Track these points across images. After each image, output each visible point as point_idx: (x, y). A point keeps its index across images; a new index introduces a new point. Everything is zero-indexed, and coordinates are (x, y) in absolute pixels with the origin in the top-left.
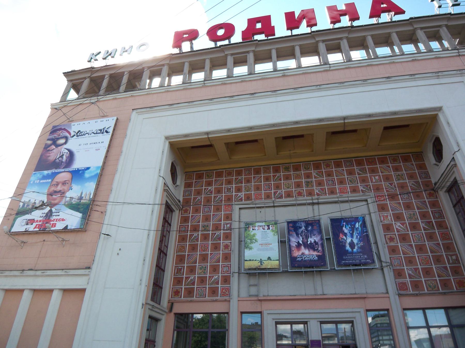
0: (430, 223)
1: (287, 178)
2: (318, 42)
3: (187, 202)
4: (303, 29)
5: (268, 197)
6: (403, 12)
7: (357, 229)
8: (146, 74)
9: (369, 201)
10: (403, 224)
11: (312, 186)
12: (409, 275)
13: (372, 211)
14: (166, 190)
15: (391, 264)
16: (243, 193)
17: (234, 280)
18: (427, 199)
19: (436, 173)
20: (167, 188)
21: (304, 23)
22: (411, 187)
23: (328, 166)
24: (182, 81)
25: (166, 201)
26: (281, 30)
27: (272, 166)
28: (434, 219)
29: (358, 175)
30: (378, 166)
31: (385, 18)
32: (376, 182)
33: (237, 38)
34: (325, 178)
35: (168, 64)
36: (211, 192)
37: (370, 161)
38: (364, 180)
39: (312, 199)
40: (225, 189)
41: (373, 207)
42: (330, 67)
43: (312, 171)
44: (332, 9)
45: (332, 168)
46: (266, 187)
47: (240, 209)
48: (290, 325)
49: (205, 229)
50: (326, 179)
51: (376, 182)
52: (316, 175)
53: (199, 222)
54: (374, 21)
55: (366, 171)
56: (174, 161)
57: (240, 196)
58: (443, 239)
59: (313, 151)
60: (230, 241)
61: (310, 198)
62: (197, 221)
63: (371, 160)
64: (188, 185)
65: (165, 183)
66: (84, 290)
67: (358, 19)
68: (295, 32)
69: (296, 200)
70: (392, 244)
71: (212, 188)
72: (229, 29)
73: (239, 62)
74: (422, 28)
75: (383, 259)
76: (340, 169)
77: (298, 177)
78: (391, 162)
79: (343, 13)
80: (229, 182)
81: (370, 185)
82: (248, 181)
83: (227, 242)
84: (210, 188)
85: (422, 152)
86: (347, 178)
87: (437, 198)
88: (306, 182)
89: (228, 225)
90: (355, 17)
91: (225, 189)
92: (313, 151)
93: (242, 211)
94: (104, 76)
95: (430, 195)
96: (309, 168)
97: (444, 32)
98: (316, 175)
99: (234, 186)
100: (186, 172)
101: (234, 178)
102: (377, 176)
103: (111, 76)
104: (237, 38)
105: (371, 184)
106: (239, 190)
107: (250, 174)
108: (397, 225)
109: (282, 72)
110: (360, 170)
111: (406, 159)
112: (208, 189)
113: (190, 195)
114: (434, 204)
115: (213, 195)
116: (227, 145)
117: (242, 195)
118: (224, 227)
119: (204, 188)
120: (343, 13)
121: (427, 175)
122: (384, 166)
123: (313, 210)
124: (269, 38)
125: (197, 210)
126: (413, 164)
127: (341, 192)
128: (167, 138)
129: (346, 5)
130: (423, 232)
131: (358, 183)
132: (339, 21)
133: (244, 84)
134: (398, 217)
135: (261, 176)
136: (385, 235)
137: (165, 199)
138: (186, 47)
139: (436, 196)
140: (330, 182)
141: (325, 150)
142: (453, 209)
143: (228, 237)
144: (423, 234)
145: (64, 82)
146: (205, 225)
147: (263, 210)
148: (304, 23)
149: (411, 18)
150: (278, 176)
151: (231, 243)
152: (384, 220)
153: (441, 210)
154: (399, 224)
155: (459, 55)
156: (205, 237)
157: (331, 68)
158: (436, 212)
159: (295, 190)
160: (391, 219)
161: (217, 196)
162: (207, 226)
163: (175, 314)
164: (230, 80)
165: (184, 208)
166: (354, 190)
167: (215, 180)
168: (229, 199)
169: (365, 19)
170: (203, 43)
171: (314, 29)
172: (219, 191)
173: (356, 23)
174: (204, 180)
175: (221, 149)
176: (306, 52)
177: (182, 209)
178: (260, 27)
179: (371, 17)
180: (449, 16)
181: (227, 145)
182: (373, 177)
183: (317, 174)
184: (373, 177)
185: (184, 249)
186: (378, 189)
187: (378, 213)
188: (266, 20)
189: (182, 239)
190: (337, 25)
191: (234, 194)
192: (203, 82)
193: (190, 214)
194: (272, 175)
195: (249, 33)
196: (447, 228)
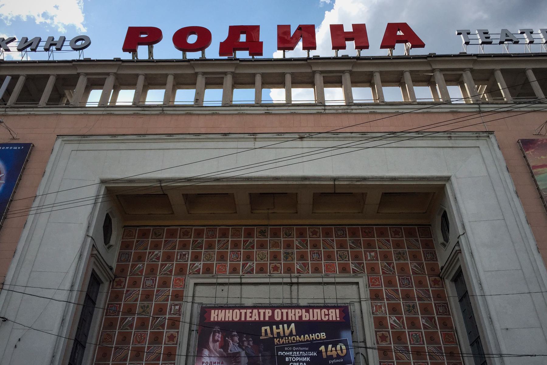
0: (432, 319)
1: (262, 246)
2: (314, 72)
3: (122, 270)
4: (299, 51)
5: (234, 270)
6: (422, 45)
8: (82, 82)
9: (361, 285)
10: (399, 318)
11: (293, 260)
13: (363, 296)
14: (95, 255)
16: (202, 263)
18: (431, 287)
19: (443, 257)
20: (95, 252)
21: (300, 44)
22: (412, 269)
23: (315, 233)
24: (131, 100)
25: (93, 270)
27: (243, 227)
28: (437, 314)
29: (351, 248)
30: (376, 239)
31: (401, 49)
32: (371, 260)
33: (212, 52)
34: (309, 250)
35: (115, 73)
36: (158, 258)
37: (367, 231)
38: (356, 257)
39: (291, 277)
40: (177, 255)
41: (365, 293)
42: (325, 110)
43: (295, 239)
44: (336, 30)
45: (320, 237)
46: (234, 256)
47: (196, 284)
48: (361, 55)
49: (144, 311)
50: (310, 251)
51: (371, 260)
52: (298, 244)
53: (136, 300)
54: (386, 52)
55: (361, 244)
56: (111, 212)
57: (197, 266)
58: (445, 342)
59: (297, 213)
60: (177, 330)
61: (288, 275)
62: (134, 299)
63: (367, 230)
64: (126, 246)
65: (93, 245)
67: (367, 47)
68: (290, 54)
69: (270, 277)
70: (384, 344)
71: (160, 253)
72: (204, 36)
73: (214, 82)
74: (441, 70)
76: (329, 239)
77: (276, 245)
78: (391, 235)
79: (349, 37)
80: (184, 246)
81: (363, 263)
82: (210, 246)
83: (172, 331)
84: (156, 252)
85: (430, 225)
86: (337, 251)
87: (443, 287)
88: (285, 253)
89: (177, 307)
90: (363, 45)
91: (177, 255)
92: (297, 213)
93: (198, 288)
95: (435, 282)
96: (290, 235)
97: (467, 76)
98: (298, 244)
99: (190, 251)
100: (125, 226)
101: (192, 240)
102: (373, 251)
104: (212, 52)
105: (365, 262)
106: (196, 258)
107: (214, 236)
108: (391, 320)
109: (266, 108)
110: (353, 243)
111: (410, 233)
112: (153, 252)
113: (128, 260)
114: (440, 296)
115: (160, 263)
116: (186, 197)
117: (199, 265)
118: (171, 309)
119: (148, 251)
120: (349, 37)
121: (434, 257)
122: (383, 239)
123: (291, 291)
124: (255, 57)
125: (135, 284)
126: (417, 241)
127: (327, 269)
128: (103, 182)
129: (354, 26)
130: (423, 331)
131: (349, 260)
132: (344, 48)
133: (215, 117)
135: (228, 241)
136: (376, 332)
137: (92, 266)
138: (142, 52)
139: (442, 284)
140: (315, 256)
141: (313, 213)
142: (458, 303)
143: (174, 323)
144: (422, 334)
146: (144, 306)
147: (226, 288)
148: (300, 44)
149: (430, 56)
150: (250, 242)
151: (178, 332)
152: (377, 311)
153: (447, 304)
154: (394, 318)
156: (143, 324)
157: (327, 111)
158: (440, 306)
159: (270, 264)
160: (386, 310)
161: (166, 264)
162: (148, 307)
164: (197, 111)
165: (117, 279)
166: (344, 269)
167: (165, 241)
168: (181, 270)
169: (375, 50)
170: (166, 50)
171: (313, 53)
172: (169, 258)
173: (365, 53)
174: (150, 240)
175: (177, 200)
176: (299, 82)
177: (114, 280)
178: (245, 40)
179: (382, 47)
180: (475, 58)
181: (186, 197)
182: (368, 253)
183: (299, 243)
184: (368, 253)
185: (111, 338)
186: (373, 270)
187: (370, 302)
188: (252, 31)
189: (110, 325)
190: (341, 53)
191: (189, 263)
192: (161, 109)
193: (124, 287)
194: (242, 239)
195: (227, 47)
196: (452, 328)
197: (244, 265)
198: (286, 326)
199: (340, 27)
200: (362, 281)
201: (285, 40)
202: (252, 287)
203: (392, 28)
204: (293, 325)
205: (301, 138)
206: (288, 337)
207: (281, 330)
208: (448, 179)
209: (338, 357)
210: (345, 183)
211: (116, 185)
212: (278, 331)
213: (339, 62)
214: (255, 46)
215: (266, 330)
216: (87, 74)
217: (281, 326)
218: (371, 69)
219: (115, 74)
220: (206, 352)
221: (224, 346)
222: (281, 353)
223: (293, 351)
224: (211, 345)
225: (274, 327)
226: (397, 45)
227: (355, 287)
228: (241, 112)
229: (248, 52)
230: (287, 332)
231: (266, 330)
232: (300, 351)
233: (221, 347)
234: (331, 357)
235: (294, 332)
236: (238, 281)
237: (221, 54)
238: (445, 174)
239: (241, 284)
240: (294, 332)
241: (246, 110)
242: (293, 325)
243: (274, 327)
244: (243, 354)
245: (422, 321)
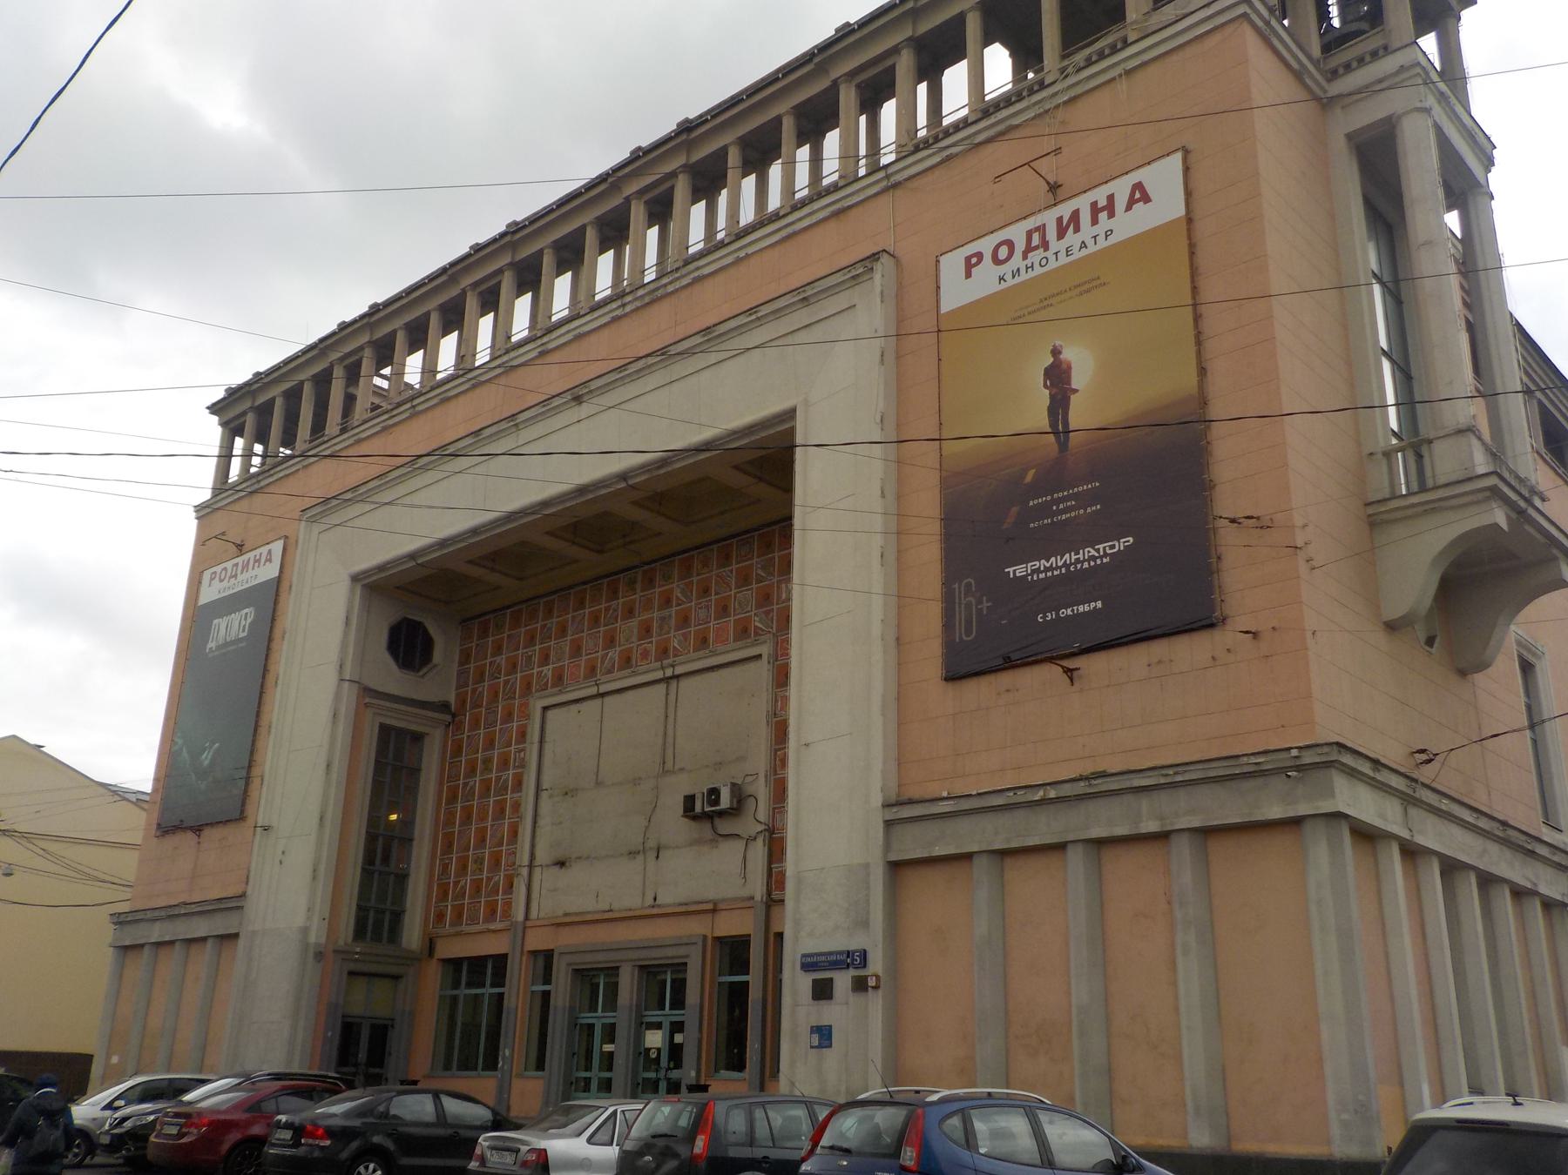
35: (684, 166)
39: (663, 668)
47: (545, 709)
64: (465, 658)
66: (236, 936)
71: (502, 660)
145: (212, 430)
163: (444, 961)
202: (617, 697)
205: (578, 400)
208: (791, 414)
210: (643, 478)
211: (772, 431)
213: (883, 26)
216: (475, 285)
219: (511, 264)
228: (789, 230)
236: (593, 691)
238: (785, 405)
241: (800, 219)
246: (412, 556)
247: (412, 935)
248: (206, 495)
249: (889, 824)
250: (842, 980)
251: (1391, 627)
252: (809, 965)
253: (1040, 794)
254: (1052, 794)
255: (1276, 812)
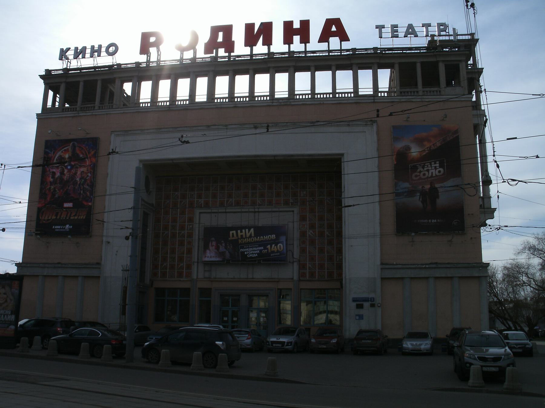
4: (260, 49)
6: (347, 39)
7: (265, 248)
12: (309, 268)
15: (299, 261)
17: (194, 268)
26: (241, 49)
39: (254, 208)
47: (200, 213)
54: (323, 46)
66: (99, 277)
75: (295, 256)
79: (296, 32)
89: (191, 226)
94: (78, 82)
103: (85, 82)
106: (200, 197)
120: (296, 32)
134: (312, 227)
143: (190, 235)
155: (374, 102)
179: (320, 41)
188: (228, 30)
191: (196, 200)
197: (227, 201)
198: (247, 230)
199: (291, 23)
200: (296, 210)
201: (250, 41)
203: (329, 22)
204: (252, 230)
205: (256, 128)
206: (248, 238)
207: (243, 233)
208: (342, 155)
209: (278, 251)
212: (242, 234)
214: (229, 45)
215: (233, 234)
217: (244, 231)
218: (309, 64)
220: (208, 251)
221: (217, 248)
222: (242, 250)
223: (249, 248)
224: (211, 248)
225: (239, 231)
226: (331, 39)
227: (292, 213)
229: (224, 49)
230: (248, 235)
231: (233, 234)
232: (253, 247)
233: (215, 249)
234: (273, 252)
235: (253, 235)
236: (224, 210)
237: (206, 53)
239: (226, 212)
240: (253, 235)
242: (252, 230)
243: (239, 231)
244: (227, 252)
245: (327, 233)
246: (172, 160)
247: (147, 281)
248: (40, 112)
249: (381, 269)
250: (366, 305)
251: (268, 131)
252: (354, 300)
253: (424, 266)
254: (427, 266)
255: (477, 275)
